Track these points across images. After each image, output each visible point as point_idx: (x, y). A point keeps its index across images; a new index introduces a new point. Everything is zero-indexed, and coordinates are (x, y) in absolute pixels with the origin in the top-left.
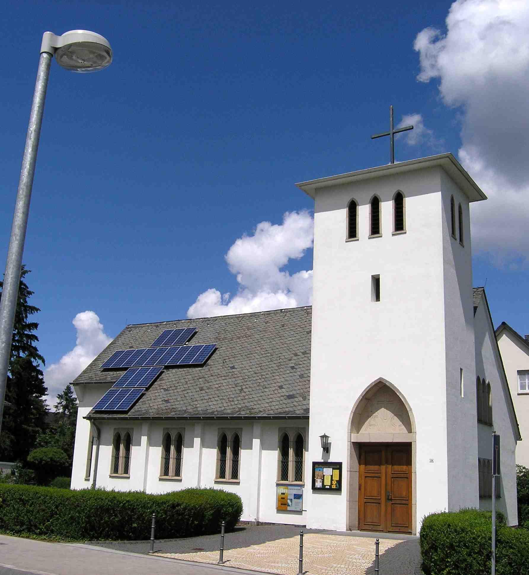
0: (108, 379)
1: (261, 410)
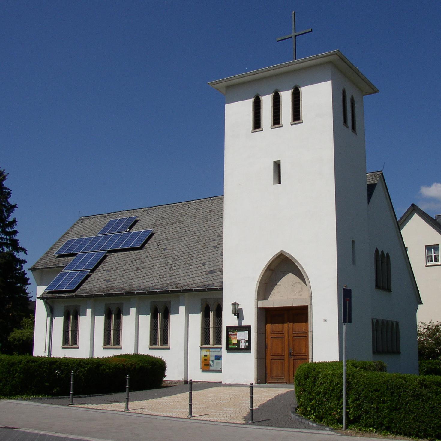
0: (60, 264)
1: (185, 284)
